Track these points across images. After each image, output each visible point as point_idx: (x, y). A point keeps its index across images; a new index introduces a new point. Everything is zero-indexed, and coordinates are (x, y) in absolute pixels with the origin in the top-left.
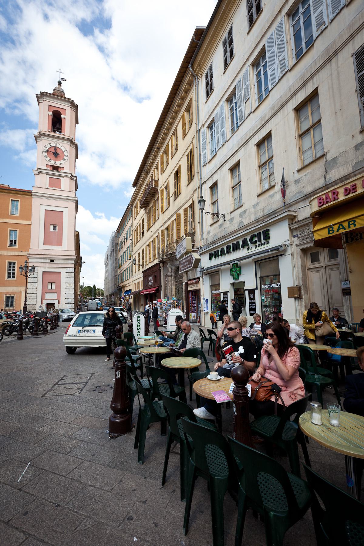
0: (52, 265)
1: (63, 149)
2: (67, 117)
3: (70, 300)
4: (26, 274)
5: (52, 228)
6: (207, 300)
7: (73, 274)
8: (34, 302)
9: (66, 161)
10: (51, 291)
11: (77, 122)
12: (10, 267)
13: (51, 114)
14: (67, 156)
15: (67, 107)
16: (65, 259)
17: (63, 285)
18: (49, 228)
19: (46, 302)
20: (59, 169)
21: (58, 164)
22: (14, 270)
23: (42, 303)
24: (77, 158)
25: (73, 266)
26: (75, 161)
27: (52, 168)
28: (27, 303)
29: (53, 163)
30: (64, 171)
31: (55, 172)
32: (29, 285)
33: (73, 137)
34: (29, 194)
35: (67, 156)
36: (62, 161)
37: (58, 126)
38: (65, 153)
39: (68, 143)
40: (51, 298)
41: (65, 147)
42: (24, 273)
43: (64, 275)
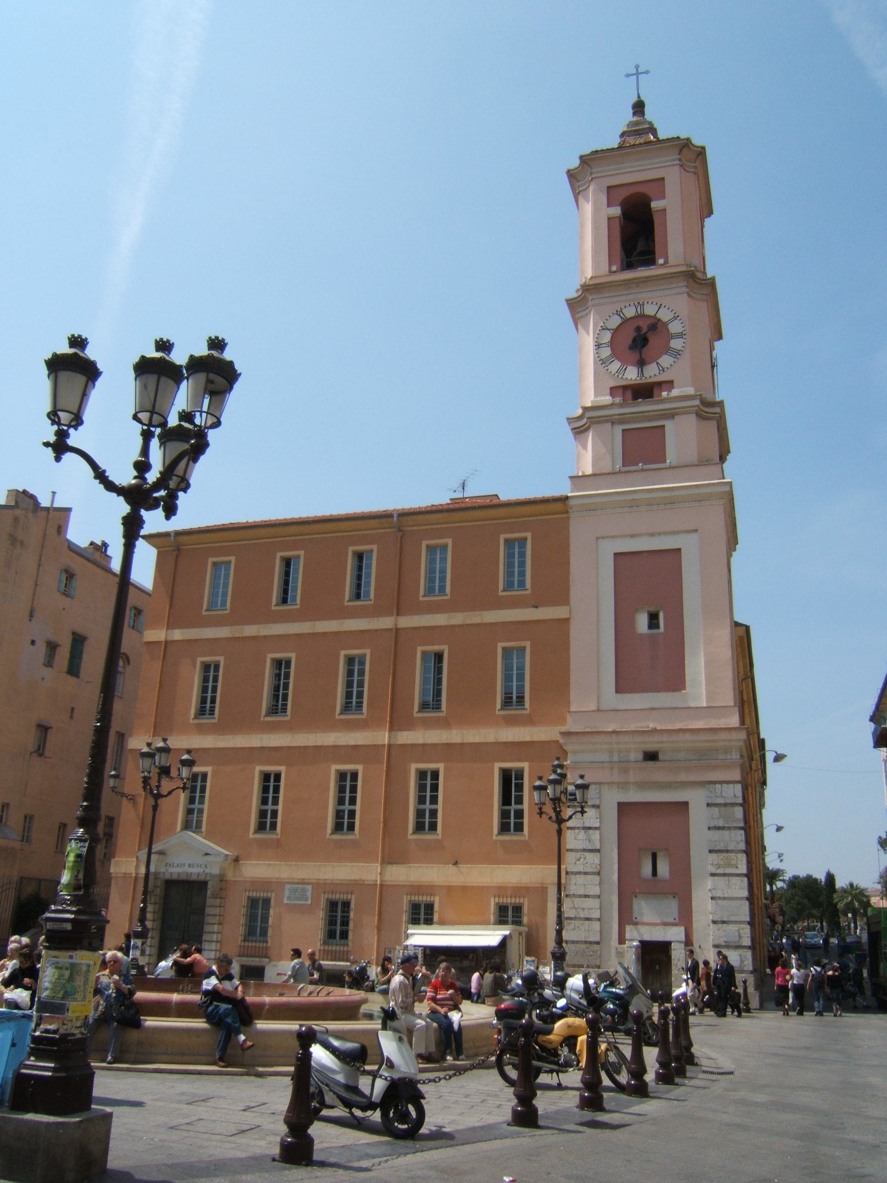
0: (655, 772)
1: (664, 315)
2: (670, 207)
3: (733, 928)
4: (558, 813)
5: (642, 621)
6: (78, 641)
7: (739, 812)
8: (593, 932)
9: (677, 354)
10: (655, 889)
11: (707, 210)
12: (265, 789)
13: (616, 211)
14: (680, 335)
15: (674, 178)
16: (705, 755)
17: (701, 861)
18: (632, 622)
19: (635, 936)
20: (656, 391)
21: (652, 373)
22: (353, 801)
23: (622, 940)
24: (720, 337)
25: (736, 775)
26: (712, 349)
27: (629, 394)
28: (565, 935)
29: (632, 375)
30: (675, 392)
31: (644, 407)
32: (570, 862)
33: (696, 262)
34: (559, 506)
35: (680, 335)
36: (665, 360)
37: (641, 246)
38: (675, 328)
39: (681, 287)
40: (654, 923)
41: (670, 306)
42: (548, 809)
43: (699, 818)
